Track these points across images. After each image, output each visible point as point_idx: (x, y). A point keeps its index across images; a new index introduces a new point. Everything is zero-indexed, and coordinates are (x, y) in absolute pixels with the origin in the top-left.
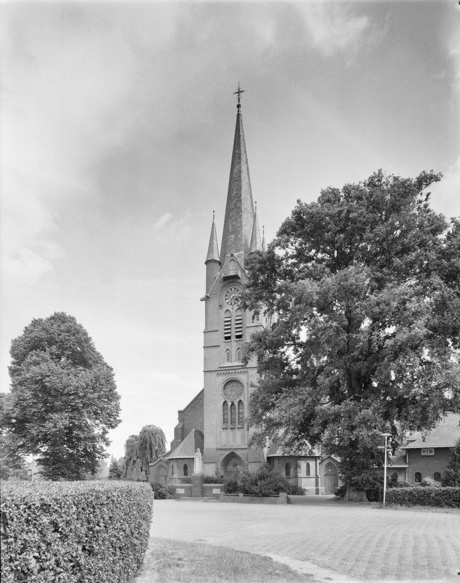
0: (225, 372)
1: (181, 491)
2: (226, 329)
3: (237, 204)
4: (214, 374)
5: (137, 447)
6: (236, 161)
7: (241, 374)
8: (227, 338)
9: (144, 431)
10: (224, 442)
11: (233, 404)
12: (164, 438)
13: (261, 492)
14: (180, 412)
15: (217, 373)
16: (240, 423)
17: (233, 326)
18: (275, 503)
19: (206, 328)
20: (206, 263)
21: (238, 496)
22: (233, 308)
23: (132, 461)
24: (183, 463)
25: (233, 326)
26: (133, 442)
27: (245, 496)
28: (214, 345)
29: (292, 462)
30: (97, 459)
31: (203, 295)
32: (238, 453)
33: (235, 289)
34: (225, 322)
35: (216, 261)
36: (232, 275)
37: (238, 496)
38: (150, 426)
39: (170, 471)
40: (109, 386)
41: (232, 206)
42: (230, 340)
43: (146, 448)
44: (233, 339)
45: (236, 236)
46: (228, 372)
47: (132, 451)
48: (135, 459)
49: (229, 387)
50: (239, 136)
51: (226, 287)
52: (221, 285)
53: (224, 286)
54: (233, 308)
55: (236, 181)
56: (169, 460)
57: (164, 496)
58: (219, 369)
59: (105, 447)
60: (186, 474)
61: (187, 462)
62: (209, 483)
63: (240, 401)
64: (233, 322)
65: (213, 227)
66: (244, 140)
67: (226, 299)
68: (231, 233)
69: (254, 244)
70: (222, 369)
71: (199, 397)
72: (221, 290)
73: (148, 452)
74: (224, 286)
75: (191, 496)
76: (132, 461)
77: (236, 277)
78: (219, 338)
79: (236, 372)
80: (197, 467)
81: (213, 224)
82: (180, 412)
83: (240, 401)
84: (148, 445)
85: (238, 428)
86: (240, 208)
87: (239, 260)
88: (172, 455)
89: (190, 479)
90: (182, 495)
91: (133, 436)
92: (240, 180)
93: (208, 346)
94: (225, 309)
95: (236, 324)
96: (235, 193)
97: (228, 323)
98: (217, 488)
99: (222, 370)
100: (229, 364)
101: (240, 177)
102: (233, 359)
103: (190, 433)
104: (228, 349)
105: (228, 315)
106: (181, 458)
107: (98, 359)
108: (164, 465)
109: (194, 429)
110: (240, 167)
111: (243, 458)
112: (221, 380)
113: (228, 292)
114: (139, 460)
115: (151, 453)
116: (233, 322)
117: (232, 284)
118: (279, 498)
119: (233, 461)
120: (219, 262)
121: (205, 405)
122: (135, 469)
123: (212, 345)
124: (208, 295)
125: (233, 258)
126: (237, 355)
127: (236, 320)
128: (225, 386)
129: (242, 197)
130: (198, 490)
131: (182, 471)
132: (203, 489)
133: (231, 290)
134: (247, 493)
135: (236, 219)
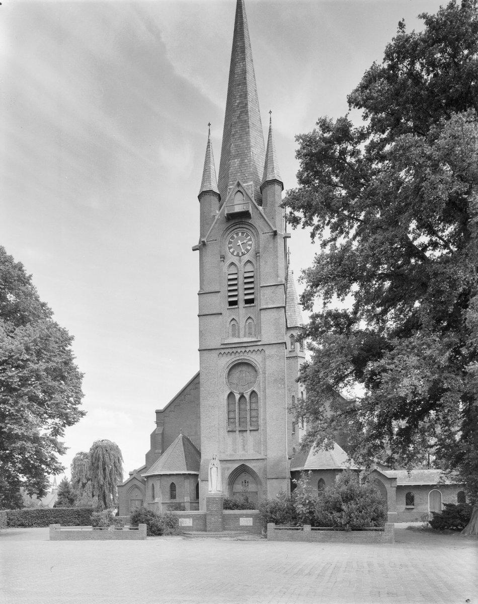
0: (230, 351)
1: (187, 522)
2: (230, 291)
3: (241, 117)
4: (214, 354)
5: (86, 468)
6: (239, 57)
7: (254, 353)
8: (232, 303)
9: (96, 447)
10: (229, 451)
11: (242, 397)
12: (121, 456)
13: (348, 523)
14: (158, 412)
15: (218, 352)
16: (253, 423)
17: (241, 287)
18: (375, 542)
19: (201, 288)
20: (200, 197)
21: (137, 529)
22: (240, 261)
23: (80, 484)
24: (167, 483)
25: (241, 287)
26: (82, 460)
27: (312, 529)
28: (214, 312)
29: (325, 478)
30: (46, 474)
31: (196, 243)
32: (250, 465)
33: (243, 233)
34: (230, 280)
35: (215, 193)
36: (239, 211)
37: (303, 529)
38: (103, 440)
39: (149, 493)
40: (64, 356)
41: (235, 119)
42: (236, 306)
43: (98, 467)
44: (241, 304)
45: (242, 161)
46: (239, 351)
47: (81, 471)
48: (85, 481)
49: (236, 373)
50: (242, 23)
51: (231, 230)
52: (224, 226)
53: (228, 229)
54: (240, 261)
55: (239, 85)
56: (147, 477)
57: (159, 530)
58: (222, 347)
59: (57, 454)
60: (173, 496)
61: (174, 480)
62: (231, 508)
63: (253, 392)
64: (241, 280)
65: (208, 146)
66: (247, 30)
67: (230, 248)
68: (235, 157)
69: (270, 170)
70: (226, 346)
71: (186, 391)
72: (223, 235)
73: (100, 472)
74: (228, 229)
75: (205, 531)
76: (80, 484)
77: (245, 215)
78: (219, 302)
79: (247, 351)
80: (213, 481)
81: (209, 142)
82: (158, 412)
83: (253, 392)
84: (100, 464)
85: (250, 430)
86: (246, 122)
87: (249, 192)
88: (152, 468)
89: (180, 504)
90: (189, 528)
91: (81, 453)
92: (245, 84)
93: (204, 313)
94: (228, 262)
95: (246, 283)
96: (238, 101)
97: (233, 282)
98: (247, 516)
99: (226, 349)
100: (236, 340)
101: (245, 78)
102: (242, 333)
103: (176, 441)
104: (233, 319)
105: (233, 270)
106: (167, 475)
107: (43, 311)
108: (139, 484)
109: (181, 435)
110: (245, 66)
111: (260, 475)
112: (226, 361)
113: (232, 238)
114: (89, 482)
115: (105, 473)
116: (241, 280)
117: (238, 226)
118: (384, 533)
119: (244, 477)
120: (219, 195)
121: (201, 399)
122: (85, 494)
123: (211, 313)
124: (204, 239)
125: (240, 189)
126: (247, 327)
127: (245, 278)
128: (229, 371)
129: (249, 107)
130: (214, 520)
131: (168, 496)
132: (224, 518)
133: (237, 234)
134: (316, 524)
135: (241, 138)
